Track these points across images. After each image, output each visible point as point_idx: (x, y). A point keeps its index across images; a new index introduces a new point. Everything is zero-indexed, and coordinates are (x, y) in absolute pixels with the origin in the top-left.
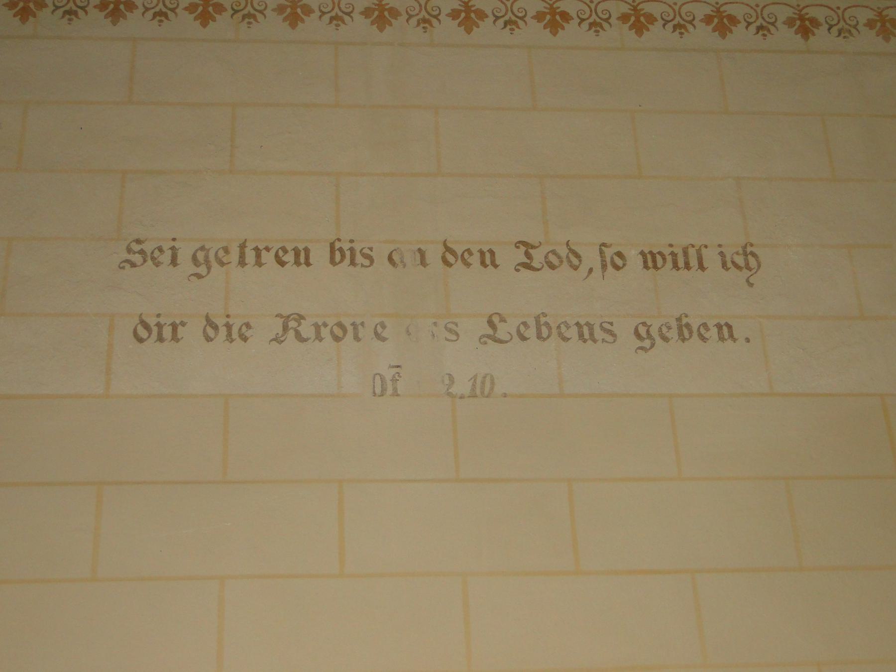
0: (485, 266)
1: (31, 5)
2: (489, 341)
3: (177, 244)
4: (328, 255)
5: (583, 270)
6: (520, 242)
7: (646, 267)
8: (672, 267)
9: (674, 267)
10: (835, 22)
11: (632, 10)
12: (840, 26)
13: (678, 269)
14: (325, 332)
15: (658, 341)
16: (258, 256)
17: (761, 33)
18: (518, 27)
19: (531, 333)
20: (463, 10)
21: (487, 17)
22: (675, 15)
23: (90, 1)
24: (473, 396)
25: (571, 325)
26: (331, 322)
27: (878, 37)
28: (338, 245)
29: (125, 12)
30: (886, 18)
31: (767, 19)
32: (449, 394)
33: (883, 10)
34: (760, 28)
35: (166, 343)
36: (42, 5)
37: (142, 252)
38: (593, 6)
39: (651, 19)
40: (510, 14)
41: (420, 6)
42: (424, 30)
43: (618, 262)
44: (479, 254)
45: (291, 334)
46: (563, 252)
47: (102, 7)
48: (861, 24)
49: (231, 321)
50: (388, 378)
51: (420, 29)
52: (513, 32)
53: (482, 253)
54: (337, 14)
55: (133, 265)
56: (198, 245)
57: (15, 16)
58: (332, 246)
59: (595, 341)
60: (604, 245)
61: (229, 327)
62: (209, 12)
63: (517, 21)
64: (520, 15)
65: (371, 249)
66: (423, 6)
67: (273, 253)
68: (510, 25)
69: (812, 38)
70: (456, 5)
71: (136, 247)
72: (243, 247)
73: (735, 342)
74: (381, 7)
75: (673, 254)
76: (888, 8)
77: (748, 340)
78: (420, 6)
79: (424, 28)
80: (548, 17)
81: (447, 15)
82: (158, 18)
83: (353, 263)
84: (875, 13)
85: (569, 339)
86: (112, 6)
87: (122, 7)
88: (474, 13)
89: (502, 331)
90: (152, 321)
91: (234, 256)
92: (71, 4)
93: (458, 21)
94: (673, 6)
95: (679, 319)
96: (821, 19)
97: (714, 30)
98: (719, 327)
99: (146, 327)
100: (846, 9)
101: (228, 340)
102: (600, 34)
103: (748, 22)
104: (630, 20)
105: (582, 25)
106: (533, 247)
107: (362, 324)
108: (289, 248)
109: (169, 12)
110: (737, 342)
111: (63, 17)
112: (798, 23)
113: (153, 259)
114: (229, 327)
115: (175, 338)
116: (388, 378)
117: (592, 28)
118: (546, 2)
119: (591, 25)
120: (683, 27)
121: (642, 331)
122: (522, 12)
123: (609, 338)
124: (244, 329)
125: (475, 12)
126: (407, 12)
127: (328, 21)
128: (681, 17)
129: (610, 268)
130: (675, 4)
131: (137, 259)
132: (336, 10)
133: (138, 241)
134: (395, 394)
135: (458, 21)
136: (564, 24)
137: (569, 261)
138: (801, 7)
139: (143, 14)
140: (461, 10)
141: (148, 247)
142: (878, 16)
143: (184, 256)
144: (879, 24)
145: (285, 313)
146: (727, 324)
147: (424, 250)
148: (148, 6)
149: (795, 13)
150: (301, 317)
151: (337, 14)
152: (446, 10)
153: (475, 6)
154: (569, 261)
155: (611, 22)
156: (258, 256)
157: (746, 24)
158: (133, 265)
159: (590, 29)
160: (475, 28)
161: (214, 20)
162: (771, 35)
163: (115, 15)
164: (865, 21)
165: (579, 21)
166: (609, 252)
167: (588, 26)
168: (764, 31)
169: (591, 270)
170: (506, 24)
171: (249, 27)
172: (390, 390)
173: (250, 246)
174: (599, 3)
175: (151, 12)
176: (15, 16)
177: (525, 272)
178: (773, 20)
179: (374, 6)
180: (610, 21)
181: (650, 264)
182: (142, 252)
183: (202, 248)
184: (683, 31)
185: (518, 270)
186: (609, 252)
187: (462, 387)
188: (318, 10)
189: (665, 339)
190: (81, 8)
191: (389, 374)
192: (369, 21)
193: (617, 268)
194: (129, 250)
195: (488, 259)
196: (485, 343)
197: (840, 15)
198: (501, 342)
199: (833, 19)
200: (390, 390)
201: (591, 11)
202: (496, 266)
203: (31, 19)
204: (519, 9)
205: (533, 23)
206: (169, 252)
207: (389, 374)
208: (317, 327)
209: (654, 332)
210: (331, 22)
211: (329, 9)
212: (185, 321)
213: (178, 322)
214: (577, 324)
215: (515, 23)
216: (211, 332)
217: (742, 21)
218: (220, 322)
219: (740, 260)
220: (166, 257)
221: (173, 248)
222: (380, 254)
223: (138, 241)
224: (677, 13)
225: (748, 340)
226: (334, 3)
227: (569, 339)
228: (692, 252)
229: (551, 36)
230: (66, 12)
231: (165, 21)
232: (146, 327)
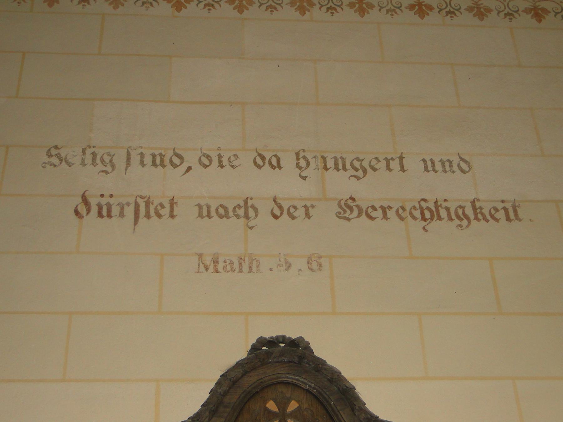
0: (338, 170)
1: (305, 4)
4: (295, 162)
7: (426, 169)
8: (386, 169)
9: (425, 170)
10: (502, 9)
11: (474, 4)
13: (428, 171)
18: (337, 12)
20: (357, 3)
21: (315, 5)
23: (284, 1)
25: (499, 209)
27: (235, 10)
30: (538, 7)
31: (513, 9)
35: (114, 219)
36: (251, 3)
37: (58, 156)
38: (506, 4)
40: (507, 9)
41: (446, 3)
42: (18, 4)
44: (385, 162)
46: (456, 160)
47: (292, 4)
48: (344, 4)
52: (452, 19)
53: (154, 156)
54: (331, 6)
56: (356, 156)
57: (234, 9)
58: (297, 154)
63: (395, 10)
64: (456, 8)
66: (448, 4)
68: (331, 10)
70: (470, 4)
71: (54, 152)
73: (498, 222)
74: (420, 4)
78: (446, 3)
79: (271, 11)
81: (465, 9)
82: (207, 8)
85: (375, 218)
86: (237, 2)
87: (244, 2)
88: (366, 4)
92: (271, 2)
94: (560, 3)
95: (473, 202)
102: (512, 20)
104: (235, 3)
105: (322, 9)
110: (500, 221)
111: (266, 10)
115: (308, 215)
117: (329, 11)
118: (474, 1)
124: (159, 208)
125: (425, 5)
126: (379, 5)
127: (385, 12)
133: (56, 147)
136: (545, 16)
139: (197, 5)
140: (474, 7)
144: (417, 7)
147: (144, 153)
149: (532, 6)
151: (331, 6)
152: (464, 7)
153: (424, 2)
155: (461, 11)
159: (327, 11)
162: (397, 15)
163: (302, 10)
165: (554, 13)
167: (203, 6)
168: (392, 12)
170: (328, 9)
171: (452, 19)
174: (509, 2)
176: (234, 9)
178: (516, 9)
179: (415, 3)
180: (460, 10)
185: (44, 167)
188: (437, 8)
192: (232, 7)
194: (50, 155)
199: (558, 9)
201: (505, 6)
203: (245, 11)
204: (514, 6)
205: (347, 9)
210: (205, 8)
212: (314, 204)
215: (453, 13)
216: (82, 210)
217: (318, 4)
223: (56, 147)
224: (506, 6)
226: (388, 2)
227: (375, 218)
231: (213, 9)
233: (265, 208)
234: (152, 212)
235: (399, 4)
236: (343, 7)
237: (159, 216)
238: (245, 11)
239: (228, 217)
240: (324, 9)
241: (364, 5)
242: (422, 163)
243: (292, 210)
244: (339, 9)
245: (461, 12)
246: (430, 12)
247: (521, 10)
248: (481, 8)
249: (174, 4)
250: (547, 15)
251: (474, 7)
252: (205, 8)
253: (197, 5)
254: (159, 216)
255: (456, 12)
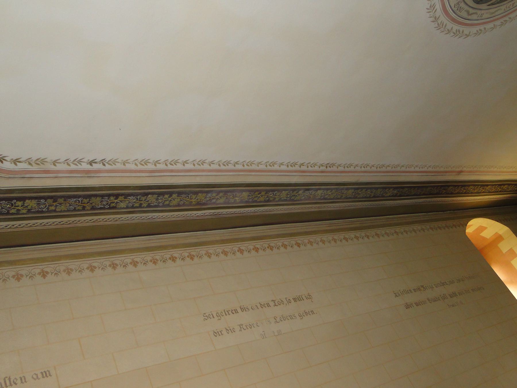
2: (277, 323)
3: (212, 313)
5: (285, 304)
6: (273, 300)
12: (316, 242)
14: (248, 327)
15: (303, 317)
16: (228, 312)
17: (103, 270)
19: (282, 319)
22: (30, 273)
24: (279, 335)
26: (248, 324)
28: (241, 307)
29: (137, 264)
32: (275, 335)
33: (43, 269)
34: (144, 264)
37: (206, 316)
39: (22, 276)
43: (289, 302)
45: (242, 329)
48: (107, 266)
49: (230, 328)
50: (263, 334)
51: (200, 259)
55: (206, 319)
59: (293, 319)
60: (286, 298)
61: (230, 329)
62: (135, 264)
65: (247, 307)
67: (230, 311)
69: (46, 278)
71: (205, 315)
72: (224, 311)
75: (298, 298)
76: (135, 258)
77: (317, 313)
80: (16, 276)
83: (246, 311)
84: (15, 273)
89: (278, 320)
90: (216, 331)
91: (224, 314)
93: (66, 273)
95: (304, 311)
96: (195, 255)
97: (66, 274)
98: (311, 311)
99: (215, 333)
100: (199, 251)
101: (21, 383)
103: (51, 272)
106: (275, 301)
107: (254, 324)
108: (233, 310)
109: (105, 268)
112: (112, 265)
113: (209, 317)
114: (230, 329)
116: (263, 334)
119: (55, 274)
120: (183, 259)
121: (35, 377)
122: (104, 264)
123: (295, 318)
125: (20, 275)
127: (29, 278)
128: (31, 274)
129: (289, 303)
130: (142, 257)
131: (206, 318)
132: (4, 277)
134: (266, 337)
135: (66, 273)
137: (282, 303)
138: (67, 266)
139: (51, 274)
141: (207, 315)
142: (41, 271)
143: (215, 315)
145: (239, 324)
146: (48, 371)
148: (27, 275)
150: (242, 325)
154: (282, 303)
156: (228, 312)
157: (51, 273)
158: (206, 319)
160: (116, 269)
161: (21, 279)
164: (169, 258)
166: (287, 299)
169: (286, 304)
172: (265, 337)
173: (226, 311)
175: (181, 259)
176: (15, 280)
177: (275, 306)
181: (295, 301)
182: (206, 316)
183: (217, 313)
184: (5, 281)
186: (287, 299)
187: (276, 334)
189: (304, 316)
190: (147, 262)
191: (263, 333)
192: (89, 270)
193: (290, 303)
195: (268, 305)
196: (276, 323)
197: (102, 264)
198: (278, 322)
200: (265, 337)
202: (238, 313)
206: (211, 315)
207: (263, 333)
208: (246, 326)
209: (301, 314)
211: (53, 271)
213: (221, 330)
214: (289, 316)
217: (97, 267)
218: (228, 329)
219: (308, 297)
220: (211, 316)
221: (212, 314)
222: (250, 307)
223: (205, 314)
225: (317, 313)
228: (300, 297)
229: (135, 268)
230: (55, 274)
232: (215, 333)
233: (224, 332)
234: (12, 383)
235: (201, 253)
236: (61, 272)
237: (16, 384)
238: (21, 280)
239: (39, 379)
240: (28, 277)
241: (19, 276)
242: (238, 312)
243: (15, 381)
244: (8, 280)
245: (128, 265)
246: (22, 278)
247: (149, 260)
248: (174, 257)
249: (42, 275)
250: (48, 274)
251: (41, 272)
252: (30, 278)
253: (51, 274)
254: (16, 384)
255: (126, 265)
